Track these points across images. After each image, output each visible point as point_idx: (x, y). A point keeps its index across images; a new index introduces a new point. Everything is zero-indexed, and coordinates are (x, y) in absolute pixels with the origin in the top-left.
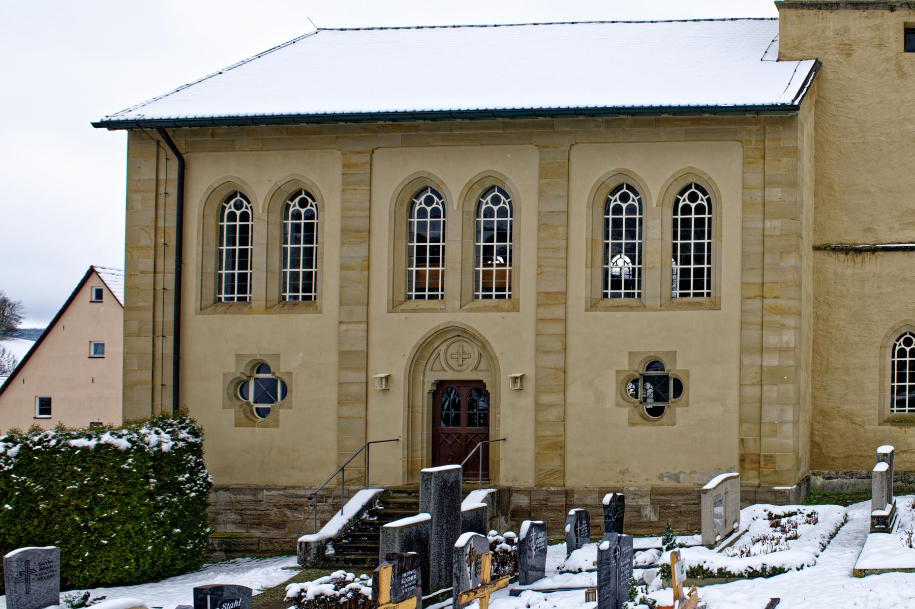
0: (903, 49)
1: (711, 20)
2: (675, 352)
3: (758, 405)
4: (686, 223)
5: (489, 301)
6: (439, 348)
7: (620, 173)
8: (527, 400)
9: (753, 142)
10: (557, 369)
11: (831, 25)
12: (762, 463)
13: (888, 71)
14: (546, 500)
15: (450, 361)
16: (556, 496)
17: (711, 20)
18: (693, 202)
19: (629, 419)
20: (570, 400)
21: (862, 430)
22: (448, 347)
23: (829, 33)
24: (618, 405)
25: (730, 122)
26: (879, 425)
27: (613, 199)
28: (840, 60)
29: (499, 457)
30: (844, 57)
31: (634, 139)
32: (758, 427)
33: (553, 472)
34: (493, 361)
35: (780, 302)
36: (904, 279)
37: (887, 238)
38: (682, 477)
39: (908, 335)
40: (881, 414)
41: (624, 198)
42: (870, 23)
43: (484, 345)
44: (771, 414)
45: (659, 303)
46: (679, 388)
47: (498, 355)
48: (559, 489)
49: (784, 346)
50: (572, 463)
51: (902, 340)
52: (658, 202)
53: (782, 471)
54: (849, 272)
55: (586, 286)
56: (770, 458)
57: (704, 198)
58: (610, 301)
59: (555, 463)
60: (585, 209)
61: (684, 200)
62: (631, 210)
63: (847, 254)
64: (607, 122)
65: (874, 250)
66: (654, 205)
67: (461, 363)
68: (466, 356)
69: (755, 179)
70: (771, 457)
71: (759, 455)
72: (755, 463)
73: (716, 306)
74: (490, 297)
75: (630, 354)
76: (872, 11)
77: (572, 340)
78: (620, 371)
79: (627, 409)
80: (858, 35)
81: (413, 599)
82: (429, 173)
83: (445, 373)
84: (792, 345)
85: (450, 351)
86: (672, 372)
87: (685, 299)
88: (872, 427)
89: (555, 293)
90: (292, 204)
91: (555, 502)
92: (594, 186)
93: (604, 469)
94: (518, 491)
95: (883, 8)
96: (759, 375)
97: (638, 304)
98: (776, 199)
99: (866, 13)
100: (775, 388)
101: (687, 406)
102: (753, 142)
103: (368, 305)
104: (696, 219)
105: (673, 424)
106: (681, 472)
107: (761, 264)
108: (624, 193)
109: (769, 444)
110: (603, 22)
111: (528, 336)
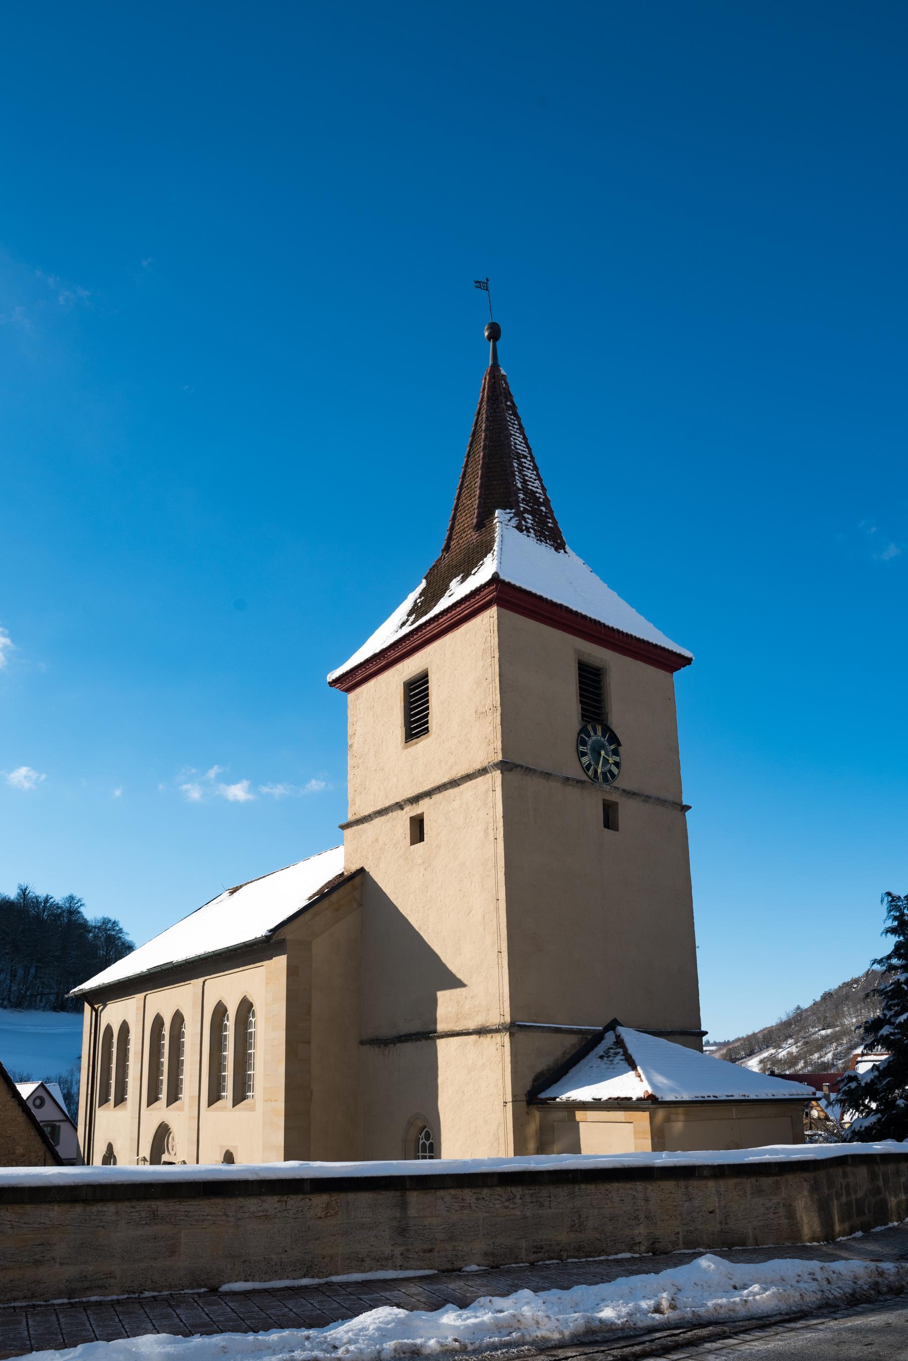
63: (379, 1047)
90: (421, 1137)
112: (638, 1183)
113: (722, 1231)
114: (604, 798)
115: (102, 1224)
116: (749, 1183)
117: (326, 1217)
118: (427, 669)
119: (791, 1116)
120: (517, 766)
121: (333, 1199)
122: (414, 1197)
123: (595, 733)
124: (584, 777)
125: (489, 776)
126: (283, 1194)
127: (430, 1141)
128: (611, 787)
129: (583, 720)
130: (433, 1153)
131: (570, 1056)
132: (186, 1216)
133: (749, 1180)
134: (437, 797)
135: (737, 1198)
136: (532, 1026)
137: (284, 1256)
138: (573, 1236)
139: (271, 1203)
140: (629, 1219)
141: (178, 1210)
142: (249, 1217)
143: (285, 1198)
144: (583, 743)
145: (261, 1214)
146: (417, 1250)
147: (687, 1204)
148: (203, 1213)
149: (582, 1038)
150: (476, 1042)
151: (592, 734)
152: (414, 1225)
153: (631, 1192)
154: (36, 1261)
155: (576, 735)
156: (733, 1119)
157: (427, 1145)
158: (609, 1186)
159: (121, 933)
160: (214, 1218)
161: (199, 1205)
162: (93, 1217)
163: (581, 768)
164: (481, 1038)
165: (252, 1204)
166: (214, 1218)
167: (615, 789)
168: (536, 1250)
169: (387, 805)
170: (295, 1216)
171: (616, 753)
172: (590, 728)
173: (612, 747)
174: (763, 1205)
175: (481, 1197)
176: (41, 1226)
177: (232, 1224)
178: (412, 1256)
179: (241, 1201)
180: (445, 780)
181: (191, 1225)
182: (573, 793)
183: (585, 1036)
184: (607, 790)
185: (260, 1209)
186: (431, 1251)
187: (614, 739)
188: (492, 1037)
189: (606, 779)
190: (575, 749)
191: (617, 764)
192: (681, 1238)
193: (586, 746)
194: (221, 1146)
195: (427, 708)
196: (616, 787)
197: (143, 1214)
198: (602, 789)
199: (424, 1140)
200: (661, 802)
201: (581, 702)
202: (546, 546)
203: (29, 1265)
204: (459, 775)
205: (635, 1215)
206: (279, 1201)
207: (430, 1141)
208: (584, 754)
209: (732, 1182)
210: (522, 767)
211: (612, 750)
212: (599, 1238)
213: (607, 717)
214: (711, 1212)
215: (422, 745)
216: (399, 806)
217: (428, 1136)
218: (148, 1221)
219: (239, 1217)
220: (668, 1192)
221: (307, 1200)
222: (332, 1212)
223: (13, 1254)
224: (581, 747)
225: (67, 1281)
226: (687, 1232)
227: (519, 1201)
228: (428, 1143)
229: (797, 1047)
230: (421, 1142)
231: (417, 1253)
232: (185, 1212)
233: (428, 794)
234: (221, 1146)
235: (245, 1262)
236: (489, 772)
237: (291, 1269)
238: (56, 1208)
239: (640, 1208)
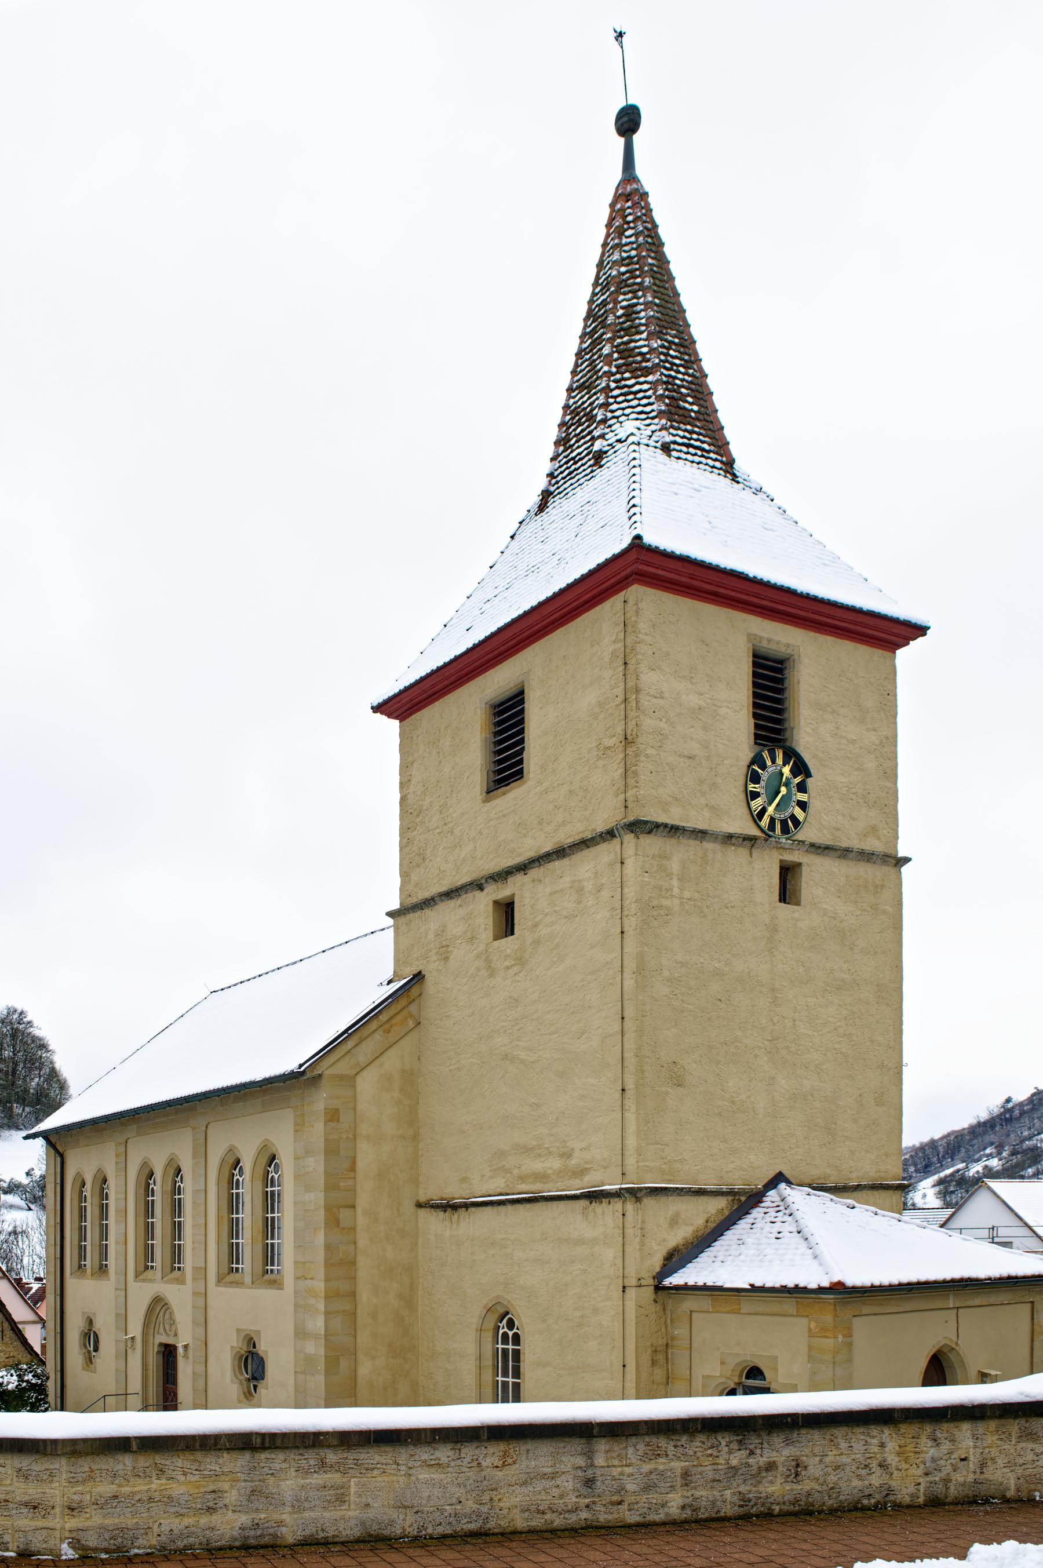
42: (462, 912)
54: (447, 1234)
63: (445, 1211)
65: (466, 1206)
76: (464, 896)
81: (910, 1145)
90: (501, 1325)
95: (473, 890)
99: (459, 901)
112: (873, 1427)
113: (975, 1481)
114: (781, 857)
115: (271, 1472)
116: (1014, 1427)
117: (504, 1465)
118: (523, 682)
119: (1032, 1302)
120: (657, 826)
121: (511, 1447)
122: (601, 1446)
123: (773, 762)
124: (755, 832)
125: (616, 841)
126: (457, 1442)
127: (515, 1330)
128: (794, 841)
129: (756, 743)
130: (519, 1345)
131: (715, 1225)
132: (355, 1464)
133: (1017, 1421)
134: (534, 873)
135: (998, 1442)
136: (666, 1188)
137: (459, 1507)
138: (788, 1488)
139: (444, 1453)
140: (858, 1468)
141: (346, 1458)
142: (421, 1466)
143: (459, 1446)
144: (755, 778)
145: (433, 1462)
146: (604, 1502)
147: (932, 1450)
148: (372, 1461)
149: (733, 1200)
150: (585, 1208)
151: (769, 763)
152: (602, 1475)
153: (862, 1437)
154: (209, 1508)
155: (744, 770)
156: (949, 1308)
157: (510, 1335)
158: (835, 1431)
159: (31, 1026)
160: (385, 1467)
161: (368, 1453)
162: (262, 1465)
163: (749, 817)
164: (594, 1204)
165: (424, 1453)
166: (385, 1467)
167: (798, 844)
168: (742, 1503)
169: (459, 884)
170: (470, 1465)
171: (802, 788)
172: (766, 754)
173: (798, 780)
174: (1032, 1450)
175: (679, 1444)
176: (212, 1473)
177: (403, 1473)
178: (598, 1509)
179: (412, 1451)
180: (548, 847)
181: (361, 1473)
182: (738, 856)
183: (737, 1198)
184: (787, 846)
185: (431, 1457)
186: (620, 1503)
187: (801, 768)
188: (609, 1203)
189: (785, 830)
190: (742, 788)
191: (802, 805)
192: (922, 1490)
193: (759, 783)
194: (238, 1330)
195: (522, 741)
196: (799, 841)
197: (312, 1462)
198: (779, 846)
199: (506, 1330)
200: (866, 856)
201: (755, 716)
202: (712, 472)
203: (202, 1511)
204: (570, 840)
205: (866, 1463)
206: (451, 1449)
207: (515, 1330)
208: (755, 795)
209: (992, 1424)
210: (666, 826)
211: (797, 784)
212: (820, 1489)
213: (793, 735)
214: (962, 1460)
215: (514, 795)
216: (478, 885)
217: (511, 1324)
218: (317, 1470)
219: (410, 1465)
220: (910, 1436)
221: (483, 1448)
222: (510, 1461)
223: (187, 1501)
224: (753, 785)
225: (240, 1528)
226: (931, 1483)
227: (726, 1449)
228: (511, 1333)
229: (1000, 1160)
230: (501, 1332)
231: (605, 1505)
232: (354, 1460)
233: (523, 868)
234: (238, 1330)
235: (417, 1512)
236: (617, 835)
237: (466, 1521)
238: (225, 1455)
239: (872, 1455)
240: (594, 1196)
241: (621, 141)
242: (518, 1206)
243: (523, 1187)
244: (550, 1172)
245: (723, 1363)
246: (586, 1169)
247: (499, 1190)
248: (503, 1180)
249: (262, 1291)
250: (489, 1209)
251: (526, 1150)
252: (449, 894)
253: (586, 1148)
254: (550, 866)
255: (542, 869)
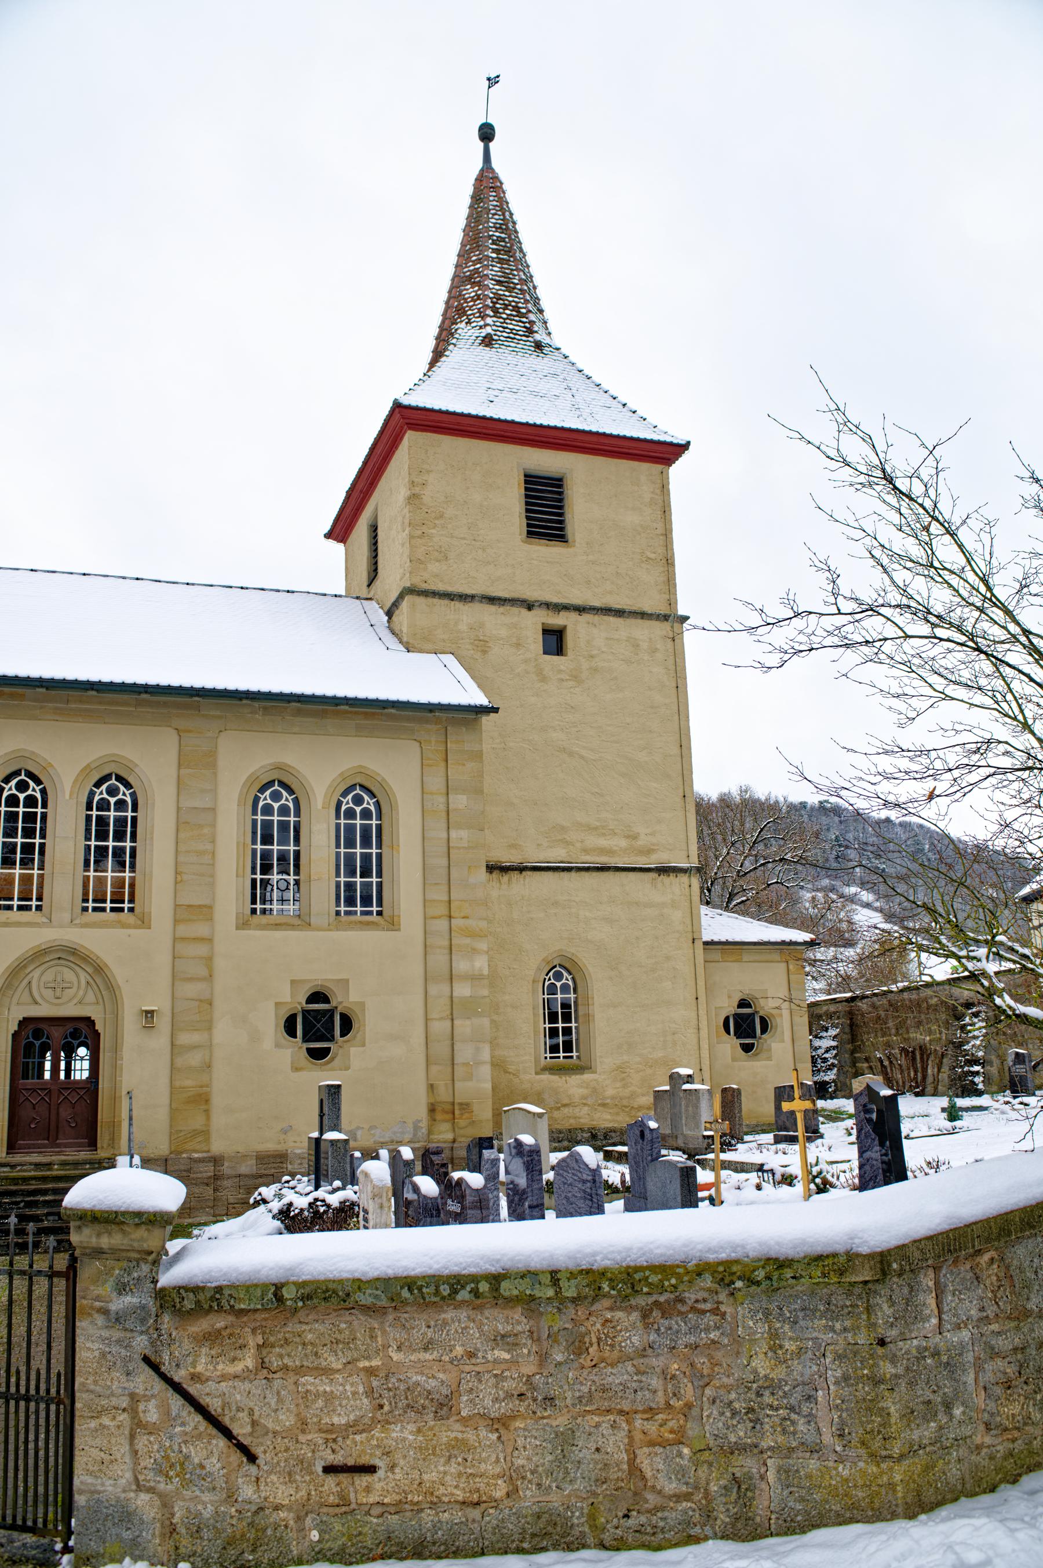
0: (542, 652)
1: (263, 589)
2: (347, 981)
3: (448, 1042)
4: (102, 821)
5: (102, 914)
6: (31, 975)
7: (279, 768)
8: (160, 1041)
9: (433, 743)
10: (201, 1001)
11: (465, 618)
12: (457, 1112)
13: (528, 673)
14: (189, 1171)
15: (43, 990)
16: (201, 1165)
17: (263, 589)
18: (276, 801)
19: (292, 1063)
20: (215, 1041)
21: (516, 1080)
22: (42, 974)
23: (463, 627)
24: (278, 1045)
25: (409, 719)
26: (537, 1073)
27: (263, 797)
28: (475, 656)
29: (120, 1116)
30: (479, 654)
31: (296, 729)
32: (449, 1069)
33: (196, 1133)
34: (111, 988)
35: (469, 922)
36: (556, 904)
37: (534, 855)
38: (359, 1133)
39: (558, 968)
40: (537, 1061)
41: (22, 786)
43: (99, 970)
44: (464, 1053)
45: (327, 921)
46: (347, 1024)
47: (121, 981)
48: (205, 1155)
49: (476, 973)
50: (219, 1120)
51: (551, 974)
52: (324, 803)
53: (481, 1121)
55: (237, 899)
56: (466, 1107)
57: (37, 788)
58: (259, 918)
59: (197, 1122)
60: (236, 807)
61: (348, 802)
62: (31, 801)
64: (265, 708)
65: (521, 869)
66: (320, 806)
67: (58, 994)
68: (68, 985)
69: (436, 782)
70: (467, 1104)
71: (453, 1104)
72: (447, 1113)
73: (393, 925)
74: (103, 910)
75: (293, 982)
77: (220, 964)
78: (280, 1003)
79: (289, 1051)
80: (494, 632)
82: (33, 753)
83: (37, 1006)
84: (486, 972)
85: (43, 978)
86: (344, 1004)
87: (352, 918)
88: (527, 1077)
89: (200, 906)
91: (201, 1172)
92: (246, 781)
93: (260, 1128)
94: (149, 1160)
96: (449, 1007)
97: (300, 923)
98: (461, 807)
99: (502, 609)
100: (468, 1022)
101: (363, 1045)
102: (433, 743)
103: (425, 900)
104: (24, 813)
105: (347, 1068)
106: (358, 1128)
107: (446, 878)
108: (22, 781)
109: (464, 1090)
110: (124, 578)
111: (164, 959)
228: (559, 984)
240: (664, 870)
241: (481, 145)
242: (583, 873)
243: (588, 858)
244: (615, 848)
245: (729, 997)
246: (653, 850)
247: (560, 859)
248: (564, 851)
249: (349, 933)
250: (550, 874)
251: (590, 829)
252: (492, 600)
253: (653, 834)
254: (606, 618)
255: (596, 617)
